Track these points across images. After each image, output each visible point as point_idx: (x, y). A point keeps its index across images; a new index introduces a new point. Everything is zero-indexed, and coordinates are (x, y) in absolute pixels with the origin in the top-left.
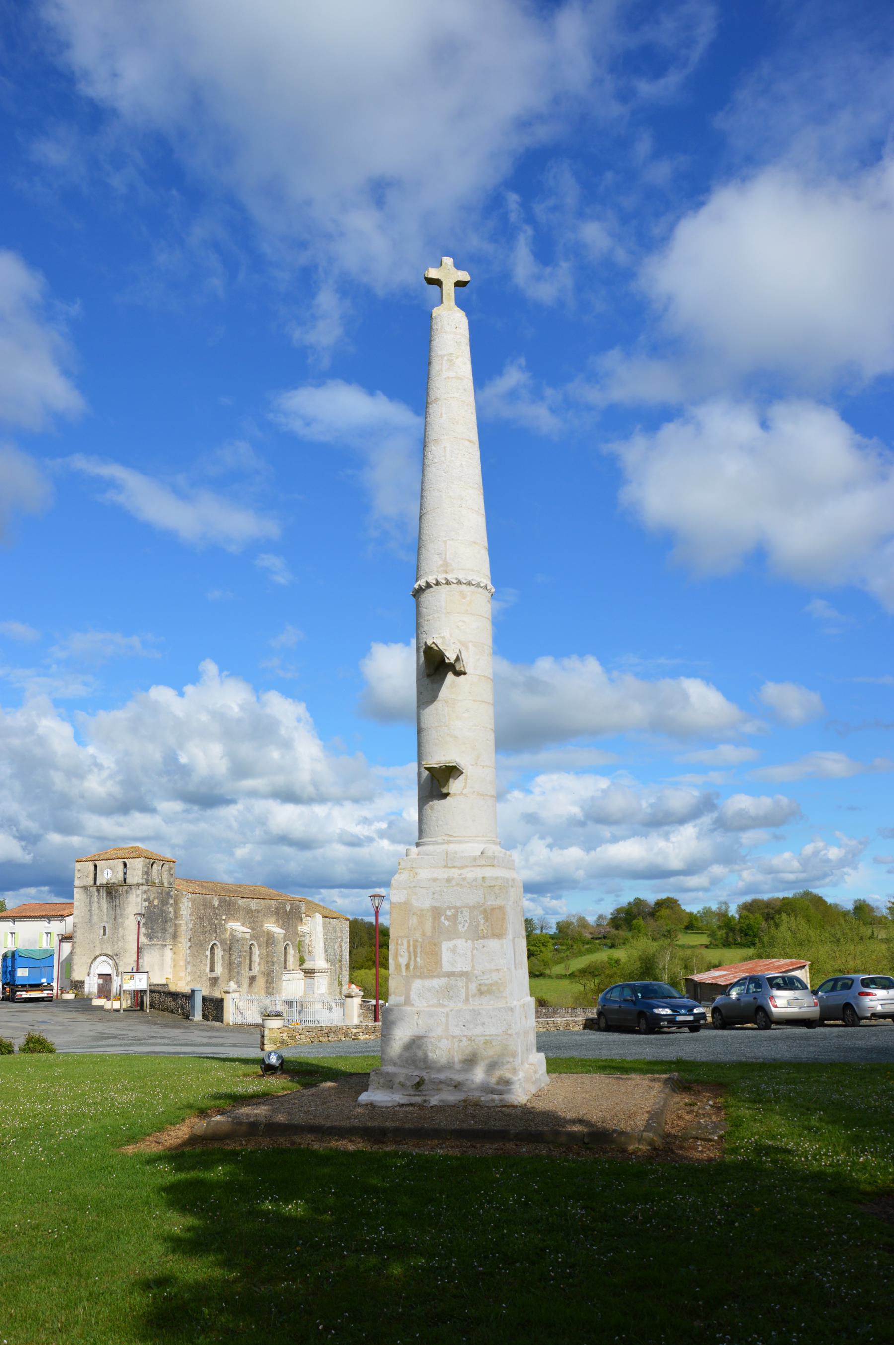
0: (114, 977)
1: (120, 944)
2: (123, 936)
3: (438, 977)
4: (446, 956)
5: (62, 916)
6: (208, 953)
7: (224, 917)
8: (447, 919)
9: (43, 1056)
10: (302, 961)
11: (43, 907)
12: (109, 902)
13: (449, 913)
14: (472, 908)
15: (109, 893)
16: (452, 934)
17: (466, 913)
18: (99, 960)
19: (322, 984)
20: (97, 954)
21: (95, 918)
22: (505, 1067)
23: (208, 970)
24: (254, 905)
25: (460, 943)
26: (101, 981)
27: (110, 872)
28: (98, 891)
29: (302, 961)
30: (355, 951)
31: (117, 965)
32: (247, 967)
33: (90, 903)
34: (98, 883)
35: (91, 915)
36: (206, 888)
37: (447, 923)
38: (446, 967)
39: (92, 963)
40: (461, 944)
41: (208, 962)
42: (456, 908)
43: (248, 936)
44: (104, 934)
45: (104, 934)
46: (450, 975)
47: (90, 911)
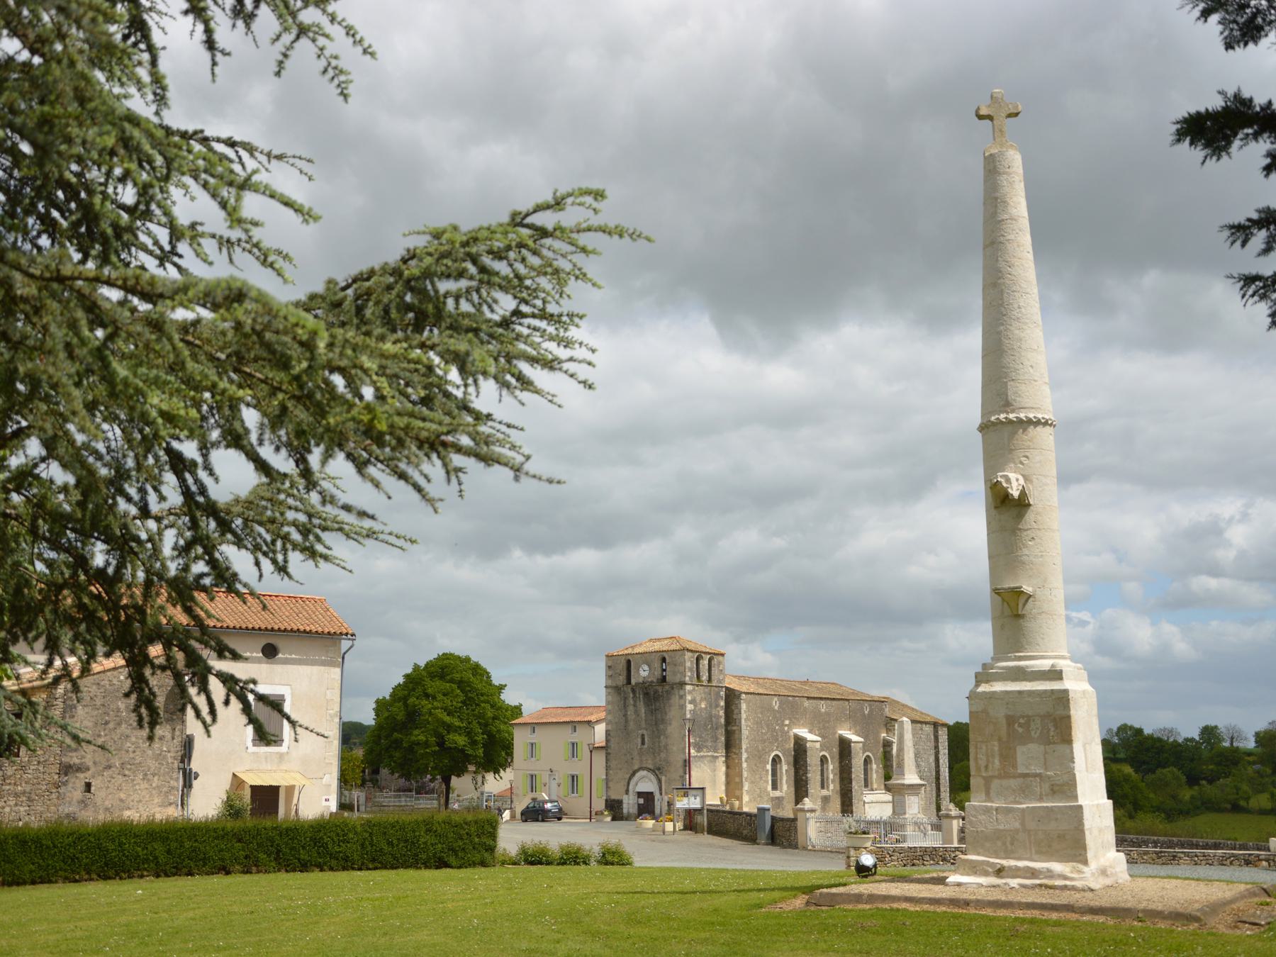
0: (657, 796)
1: (663, 755)
2: (666, 746)
3: (1014, 777)
4: (1020, 758)
5: (589, 722)
6: (769, 767)
7: (787, 722)
8: (1020, 725)
9: (624, 869)
10: (888, 777)
11: (567, 711)
12: (647, 704)
13: (1022, 721)
14: (1043, 717)
15: (646, 694)
16: (1025, 739)
17: (1038, 721)
18: (638, 775)
19: (915, 807)
20: (636, 767)
21: (632, 725)
22: (149, 224)
23: (769, 788)
24: (823, 707)
25: (1032, 746)
26: (641, 801)
27: (646, 667)
28: (633, 691)
29: (888, 777)
30: (957, 766)
31: (660, 781)
32: (819, 784)
33: (625, 706)
34: (633, 682)
35: (627, 721)
36: (763, 686)
37: (1020, 730)
38: (1021, 770)
39: (630, 779)
40: (1034, 749)
41: (770, 778)
42: (1028, 716)
43: (818, 745)
44: (643, 743)
45: (643, 743)
46: (1025, 776)
47: (625, 715)
